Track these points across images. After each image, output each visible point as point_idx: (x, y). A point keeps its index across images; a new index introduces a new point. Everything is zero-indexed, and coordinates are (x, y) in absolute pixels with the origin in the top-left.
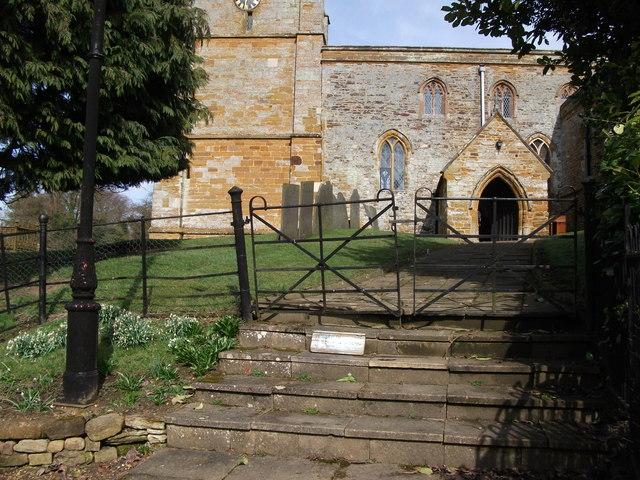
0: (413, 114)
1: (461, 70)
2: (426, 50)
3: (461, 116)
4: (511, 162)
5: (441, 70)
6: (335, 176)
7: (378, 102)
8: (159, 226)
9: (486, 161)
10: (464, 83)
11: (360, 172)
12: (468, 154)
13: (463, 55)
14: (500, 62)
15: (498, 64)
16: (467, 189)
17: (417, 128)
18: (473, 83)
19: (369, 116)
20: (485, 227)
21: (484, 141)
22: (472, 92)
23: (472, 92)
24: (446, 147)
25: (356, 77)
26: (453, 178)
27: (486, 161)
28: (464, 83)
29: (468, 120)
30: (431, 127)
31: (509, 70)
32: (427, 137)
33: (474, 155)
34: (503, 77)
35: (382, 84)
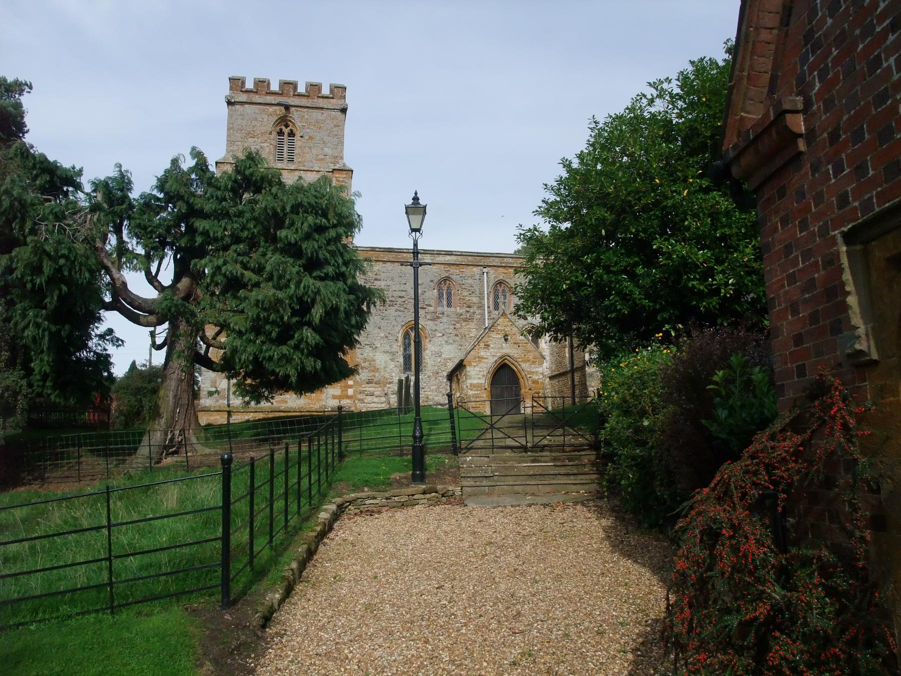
0: (430, 308)
1: (468, 271)
2: (439, 253)
3: (468, 309)
4: (516, 351)
5: (452, 271)
6: (365, 360)
7: (400, 297)
8: (207, 405)
9: (496, 351)
10: (470, 281)
11: (387, 357)
12: (482, 345)
13: (470, 258)
14: (499, 264)
15: (498, 266)
16: (482, 373)
17: (433, 320)
18: (478, 282)
19: (393, 309)
20: (495, 401)
21: (494, 335)
22: (477, 288)
23: (477, 288)
24: (456, 335)
25: (382, 274)
26: (470, 365)
27: (496, 351)
28: (470, 281)
29: (474, 313)
30: (444, 319)
31: (506, 271)
32: (441, 327)
33: (487, 346)
34: (501, 277)
35: (404, 282)
